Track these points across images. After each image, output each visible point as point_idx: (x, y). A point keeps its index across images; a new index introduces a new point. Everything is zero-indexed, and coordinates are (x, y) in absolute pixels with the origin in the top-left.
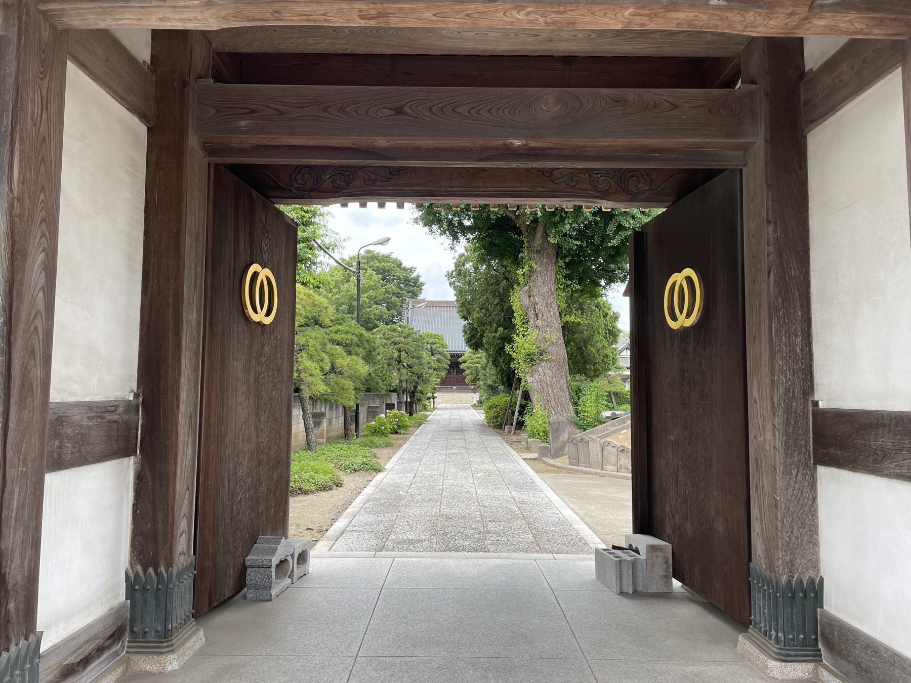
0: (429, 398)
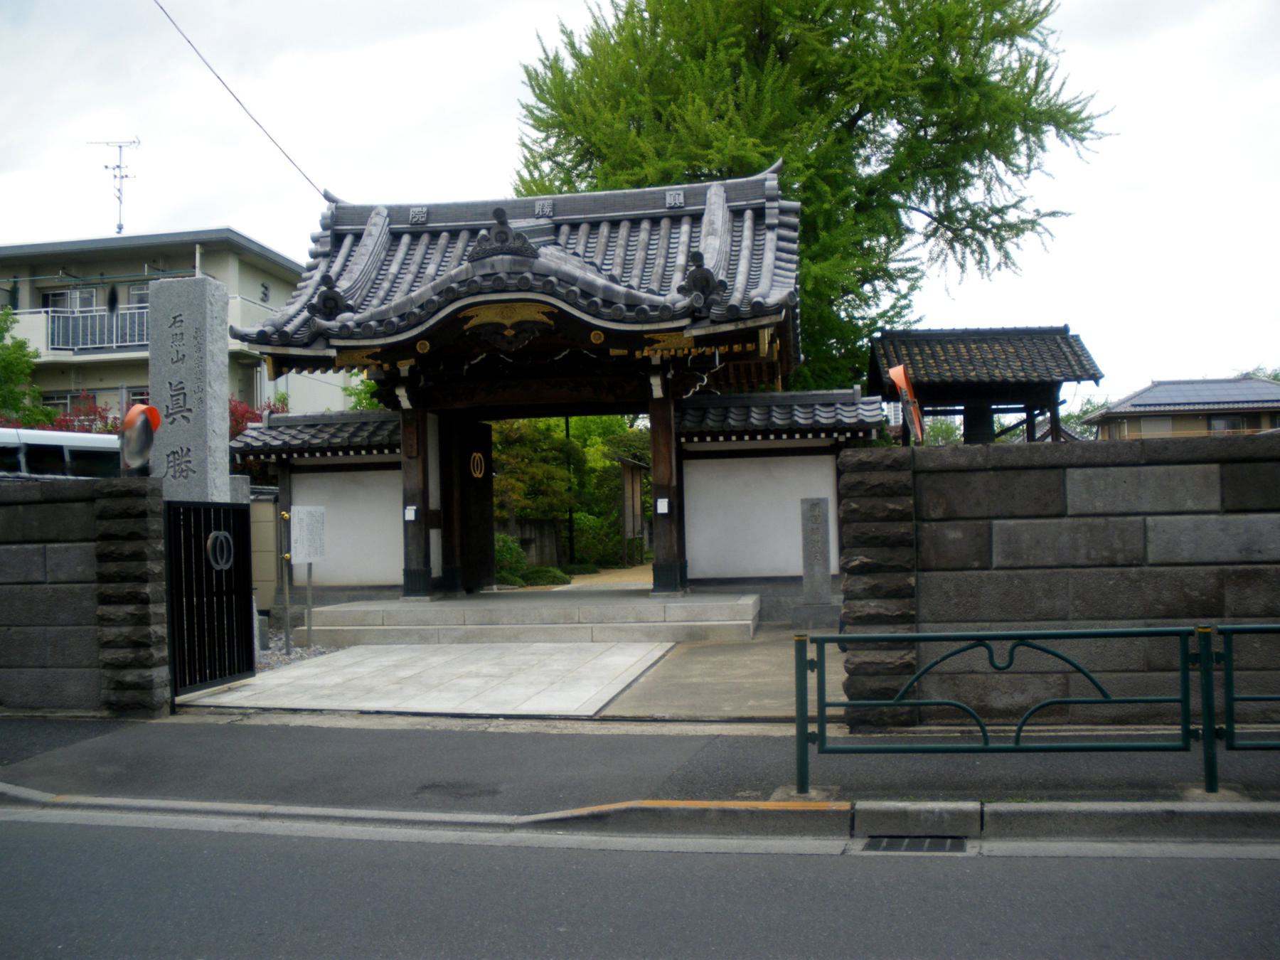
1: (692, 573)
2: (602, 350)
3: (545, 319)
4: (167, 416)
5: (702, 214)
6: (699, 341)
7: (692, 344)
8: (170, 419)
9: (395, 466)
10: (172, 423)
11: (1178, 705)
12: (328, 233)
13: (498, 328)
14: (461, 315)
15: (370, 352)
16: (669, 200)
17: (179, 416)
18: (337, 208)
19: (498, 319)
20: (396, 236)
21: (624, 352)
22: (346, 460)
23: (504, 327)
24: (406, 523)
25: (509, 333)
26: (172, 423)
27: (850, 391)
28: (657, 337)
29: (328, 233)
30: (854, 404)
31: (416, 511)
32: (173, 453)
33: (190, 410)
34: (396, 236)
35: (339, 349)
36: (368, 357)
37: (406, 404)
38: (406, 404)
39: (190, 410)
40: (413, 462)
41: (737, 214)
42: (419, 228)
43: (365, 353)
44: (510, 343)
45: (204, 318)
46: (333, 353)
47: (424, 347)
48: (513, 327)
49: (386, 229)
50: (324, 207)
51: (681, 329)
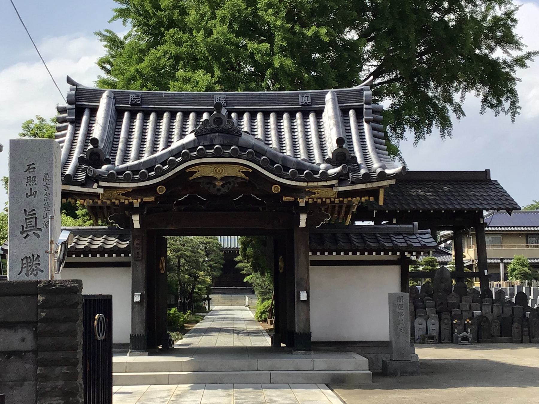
0: (205, 299)
1: (314, 337)
2: (279, 196)
3: (243, 175)
4: (22, 233)
5: (323, 111)
6: (340, 194)
7: (336, 195)
8: (25, 235)
9: (125, 265)
10: (25, 238)
11: (256, 368)
12: (73, 107)
13: (211, 180)
14: (188, 171)
15: (121, 191)
16: (301, 100)
17: (32, 232)
18: (77, 89)
19: (212, 174)
20: (119, 113)
21: (292, 199)
22: (86, 260)
23: (215, 179)
24: (134, 304)
25: (219, 184)
26: (25, 238)
27: (411, 226)
28: (316, 191)
29: (73, 107)
30: (414, 234)
31: (141, 296)
32: (26, 257)
33: (40, 229)
34: (119, 113)
35: (105, 188)
36: (123, 194)
37: (137, 225)
38: (137, 225)
39: (40, 229)
40: (138, 263)
41: (345, 112)
42: (136, 108)
43: (121, 191)
44: (219, 190)
45: (52, 167)
46: (101, 191)
47: (162, 190)
48: (222, 179)
49: (114, 108)
50: (67, 89)
51: (332, 186)
